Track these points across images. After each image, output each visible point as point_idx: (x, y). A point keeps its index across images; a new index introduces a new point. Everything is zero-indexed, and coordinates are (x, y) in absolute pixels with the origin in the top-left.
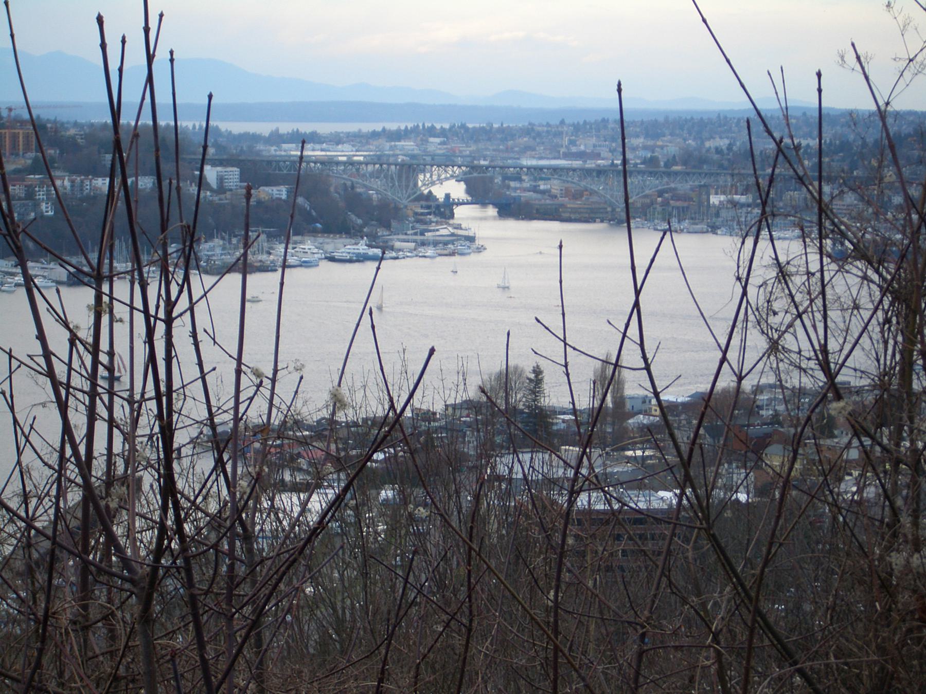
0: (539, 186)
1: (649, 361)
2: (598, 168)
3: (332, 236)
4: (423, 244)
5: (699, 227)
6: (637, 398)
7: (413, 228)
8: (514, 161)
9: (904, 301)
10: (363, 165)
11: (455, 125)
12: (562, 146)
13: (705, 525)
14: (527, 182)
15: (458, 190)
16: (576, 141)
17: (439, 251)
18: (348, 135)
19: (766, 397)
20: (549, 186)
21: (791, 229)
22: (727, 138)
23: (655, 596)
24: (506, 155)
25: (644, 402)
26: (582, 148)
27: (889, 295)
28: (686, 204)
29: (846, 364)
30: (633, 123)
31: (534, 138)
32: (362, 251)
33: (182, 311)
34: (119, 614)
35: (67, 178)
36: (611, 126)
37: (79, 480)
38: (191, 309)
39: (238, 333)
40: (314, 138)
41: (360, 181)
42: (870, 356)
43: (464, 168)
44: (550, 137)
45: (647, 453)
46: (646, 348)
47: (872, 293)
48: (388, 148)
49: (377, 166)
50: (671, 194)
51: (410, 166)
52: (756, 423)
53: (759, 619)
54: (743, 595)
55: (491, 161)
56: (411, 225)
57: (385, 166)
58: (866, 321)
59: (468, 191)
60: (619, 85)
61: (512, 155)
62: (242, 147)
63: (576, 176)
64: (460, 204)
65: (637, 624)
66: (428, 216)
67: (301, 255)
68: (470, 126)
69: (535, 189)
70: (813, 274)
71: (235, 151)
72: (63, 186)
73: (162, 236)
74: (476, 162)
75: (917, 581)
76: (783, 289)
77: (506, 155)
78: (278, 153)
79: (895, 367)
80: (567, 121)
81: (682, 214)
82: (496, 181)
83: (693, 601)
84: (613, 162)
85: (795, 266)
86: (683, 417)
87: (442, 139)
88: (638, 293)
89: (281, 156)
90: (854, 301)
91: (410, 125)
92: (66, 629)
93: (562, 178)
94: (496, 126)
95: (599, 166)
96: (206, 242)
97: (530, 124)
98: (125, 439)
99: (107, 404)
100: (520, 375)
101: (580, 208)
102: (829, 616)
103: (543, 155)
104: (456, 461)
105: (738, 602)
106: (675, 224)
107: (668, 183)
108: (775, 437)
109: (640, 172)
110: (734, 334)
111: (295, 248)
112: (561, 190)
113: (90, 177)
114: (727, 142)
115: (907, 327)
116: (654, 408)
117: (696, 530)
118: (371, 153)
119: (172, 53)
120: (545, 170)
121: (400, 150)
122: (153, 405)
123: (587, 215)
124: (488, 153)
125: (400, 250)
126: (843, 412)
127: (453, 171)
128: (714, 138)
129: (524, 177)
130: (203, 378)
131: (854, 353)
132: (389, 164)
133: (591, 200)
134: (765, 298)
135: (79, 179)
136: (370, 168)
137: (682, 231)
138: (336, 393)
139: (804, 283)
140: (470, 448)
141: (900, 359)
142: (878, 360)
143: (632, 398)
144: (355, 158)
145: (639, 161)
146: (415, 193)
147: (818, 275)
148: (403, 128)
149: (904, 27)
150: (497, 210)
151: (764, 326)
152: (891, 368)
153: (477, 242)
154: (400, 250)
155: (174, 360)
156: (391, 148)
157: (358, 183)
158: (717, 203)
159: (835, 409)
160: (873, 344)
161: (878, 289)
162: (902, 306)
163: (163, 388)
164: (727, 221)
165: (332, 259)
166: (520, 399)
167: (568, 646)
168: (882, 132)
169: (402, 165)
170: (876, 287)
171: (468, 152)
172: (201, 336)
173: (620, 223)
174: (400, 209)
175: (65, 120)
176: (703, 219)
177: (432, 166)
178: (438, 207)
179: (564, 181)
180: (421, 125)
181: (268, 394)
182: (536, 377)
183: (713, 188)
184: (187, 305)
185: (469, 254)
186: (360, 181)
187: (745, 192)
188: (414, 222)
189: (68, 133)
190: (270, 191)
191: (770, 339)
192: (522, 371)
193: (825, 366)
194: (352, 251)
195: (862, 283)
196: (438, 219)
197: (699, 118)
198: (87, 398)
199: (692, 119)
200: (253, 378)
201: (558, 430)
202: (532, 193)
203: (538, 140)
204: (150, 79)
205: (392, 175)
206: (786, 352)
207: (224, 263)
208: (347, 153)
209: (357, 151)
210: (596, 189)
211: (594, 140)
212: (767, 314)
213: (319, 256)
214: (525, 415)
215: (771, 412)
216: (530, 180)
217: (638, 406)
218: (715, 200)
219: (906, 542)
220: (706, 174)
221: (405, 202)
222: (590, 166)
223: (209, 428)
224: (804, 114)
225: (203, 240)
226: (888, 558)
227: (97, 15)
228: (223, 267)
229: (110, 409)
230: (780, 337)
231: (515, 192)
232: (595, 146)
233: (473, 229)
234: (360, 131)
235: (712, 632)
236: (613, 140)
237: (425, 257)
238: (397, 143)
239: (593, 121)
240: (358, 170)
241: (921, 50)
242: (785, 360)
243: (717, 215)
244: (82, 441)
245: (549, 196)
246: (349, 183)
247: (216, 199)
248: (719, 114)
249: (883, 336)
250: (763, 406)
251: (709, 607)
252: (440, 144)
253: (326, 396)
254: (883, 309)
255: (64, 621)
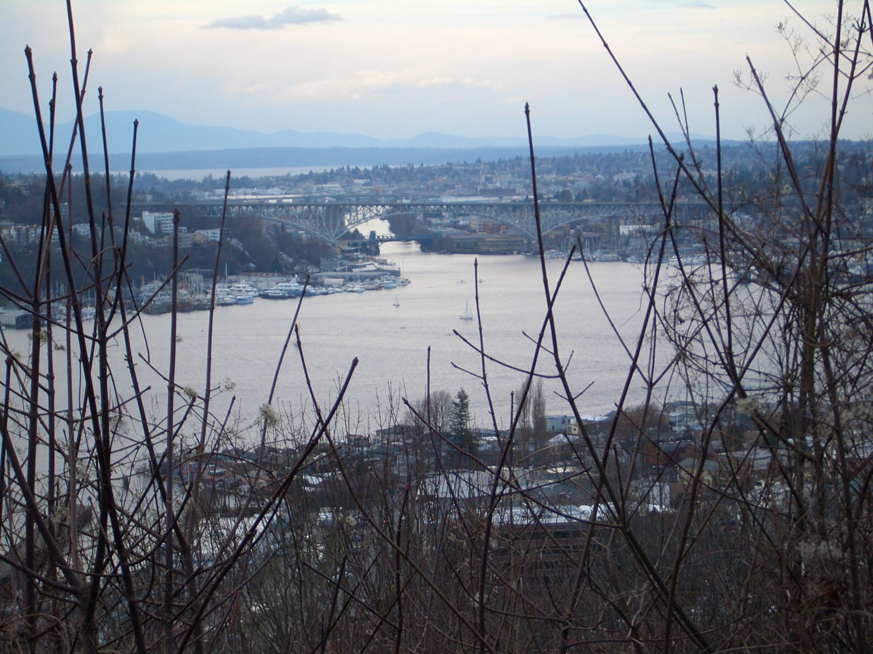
0: (459, 222)
1: (564, 369)
2: (514, 203)
3: (265, 274)
4: (351, 279)
5: (610, 256)
6: (557, 418)
7: (341, 265)
8: (434, 199)
9: (804, 306)
10: (293, 207)
11: (377, 166)
12: (479, 184)
13: (621, 525)
14: (447, 218)
15: (382, 228)
16: (492, 178)
17: (366, 286)
18: (277, 179)
19: (678, 414)
20: (468, 222)
21: (696, 255)
22: (634, 171)
23: (576, 594)
24: (426, 193)
25: (564, 422)
26: (498, 184)
27: (789, 301)
28: (597, 235)
29: (749, 367)
30: (546, 160)
31: (453, 177)
32: (293, 288)
33: (115, 331)
34: (63, 624)
35: (13, 227)
36: (524, 164)
37: (24, 501)
38: (125, 328)
39: (169, 357)
40: (245, 183)
41: (291, 222)
42: (773, 360)
43: (387, 207)
44: (467, 176)
45: (568, 470)
46: (559, 357)
47: (773, 299)
48: (315, 190)
49: (306, 207)
50: (583, 226)
51: (336, 206)
52: (670, 439)
53: (675, 613)
54: (660, 590)
55: (413, 200)
56: (339, 262)
57: (313, 207)
58: (767, 325)
59: (392, 229)
60: (527, 106)
61: (433, 194)
62: (177, 194)
63: (493, 211)
64: (383, 241)
65: (560, 622)
66: (356, 253)
67: (235, 293)
68: (392, 167)
69: (455, 225)
70: (717, 283)
71: (171, 197)
72: (9, 234)
73: (94, 259)
74: (398, 201)
75: (825, 568)
76: (689, 298)
77: (426, 193)
78: (212, 198)
79: (797, 369)
80: (483, 160)
81: (595, 244)
82: (418, 218)
83: (612, 598)
84: (527, 197)
85: (699, 276)
86: (601, 435)
87: (366, 181)
88: (550, 304)
89: (214, 201)
90: (757, 308)
91: (336, 168)
92: (14, 642)
93: (480, 214)
94: (416, 166)
95: (514, 201)
96: (146, 284)
97: (448, 164)
98: (66, 461)
99: (48, 427)
100: (446, 401)
101: (497, 241)
102: (741, 608)
103: (462, 193)
104: (387, 483)
105: (655, 597)
106: (587, 254)
107: (580, 216)
108: (689, 451)
109: (554, 206)
110: (643, 343)
111: (231, 287)
112: (480, 225)
113: (35, 226)
114: (634, 175)
115: (806, 329)
116: (573, 427)
117: (613, 529)
118: (300, 196)
119: (100, 90)
120: (464, 207)
121: (327, 192)
122: (89, 424)
123: (504, 248)
124: (410, 192)
125: (329, 286)
126: (750, 408)
127: (377, 210)
128: (622, 172)
129: (444, 214)
130: (138, 396)
131: (756, 357)
132: (317, 206)
133: (508, 234)
134: (672, 307)
135: (24, 228)
136: (299, 209)
137: (594, 260)
138: (267, 410)
139: (708, 292)
140: (400, 470)
141: (802, 362)
142: (781, 364)
143: (552, 419)
144: (285, 201)
145: (551, 196)
146: (342, 232)
147: (721, 282)
148: (329, 171)
149: (796, 46)
150: (420, 245)
151: (671, 333)
152: (793, 371)
153: (402, 276)
154: (329, 286)
155: (109, 379)
156: (319, 190)
157: (288, 224)
158: (626, 233)
159: (742, 406)
160: (775, 348)
161: (779, 296)
162: (802, 311)
163: (99, 408)
164: (636, 249)
165: (266, 296)
166: (446, 423)
167: (495, 644)
168: (778, 148)
169: (329, 206)
170: (776, 293)
171: (391, 192)
172: (136, 359)
173: (534, 255)
174: (328, 247)
175: (9, 172)
176: (614, 249)
177: (357, 206)
178: (364, 244)
179: (482, 216)
180: (345, 168)
181: (201, 412)
182: (461, 401)
183: (622, 219)
184: (121, 324)
185: (395, 287)
186: (291, 222)
187: (653, 223)
188: (342, 259)
189: (13, 185)
190: (205, 234)
191: (678, 346)
192: (448, 396)
193: (730, 369)
194: (285, 288)
195: (763, 291)
196: (364, 255)
197: (607, 153)
198: (28, 420)
199: (600, 154)
200: (187, 397)
201: (483, 451)
202: (452, 229)
203: (456, 179)
204: (79, 119)
205: (320, 216)
206: (694, 358)
207: (164, 303)
208: (277, 196)
209: (286, 194)
210: (512, 223)
211: (509, 177)
212: (675, 323)
213: (253, 293)
214: (452, 438)
215: (683, 428)
216: (451, 216)
217: (558, 426)
218: (624, 230)
219: (813, 531)
220: (615, 206)
221: (332, 240)
222: (506, 201)
223: (145, 447)
224: (706, 147)
225: (143, 282)
226: (796, 548)
227: (25, 48)
228: (163, 307)
229: (51, 432)
230: (687, 344)
231: (437, 228)
232: (510, 183)
233: (397, 264)
234: (288, 175)
235: (631, 627)
236: (526, 177)
237: (353, 291)
238: (324, 186)
239: (507, 159)
240: (287, 212)
241: (813, 68)
242: (693, 366)
243: (627, 244)
244: (24, 463)
245: (468, 231)
246: (279, 224)
247: (154, 243)
248: (626, 150)
249: (785, 339)
250: (675, 422)
251: (628, 604)
252: (365, 185)
253: (256, 414)
254: (784, 315)
255: (11, 633)
